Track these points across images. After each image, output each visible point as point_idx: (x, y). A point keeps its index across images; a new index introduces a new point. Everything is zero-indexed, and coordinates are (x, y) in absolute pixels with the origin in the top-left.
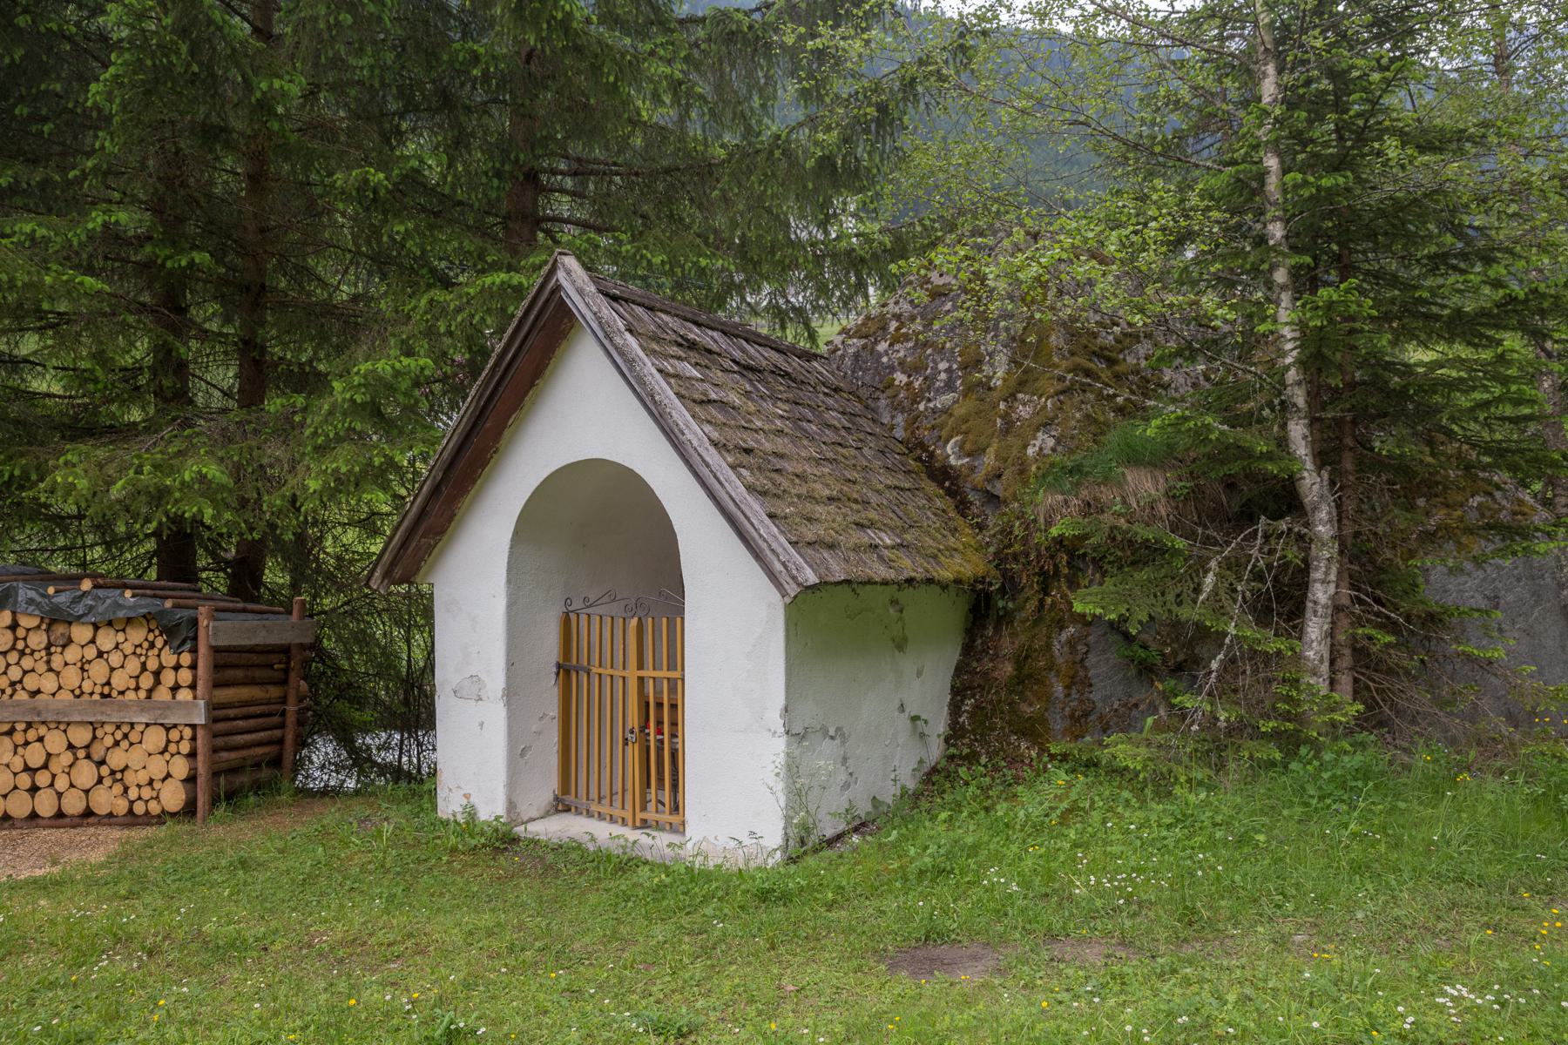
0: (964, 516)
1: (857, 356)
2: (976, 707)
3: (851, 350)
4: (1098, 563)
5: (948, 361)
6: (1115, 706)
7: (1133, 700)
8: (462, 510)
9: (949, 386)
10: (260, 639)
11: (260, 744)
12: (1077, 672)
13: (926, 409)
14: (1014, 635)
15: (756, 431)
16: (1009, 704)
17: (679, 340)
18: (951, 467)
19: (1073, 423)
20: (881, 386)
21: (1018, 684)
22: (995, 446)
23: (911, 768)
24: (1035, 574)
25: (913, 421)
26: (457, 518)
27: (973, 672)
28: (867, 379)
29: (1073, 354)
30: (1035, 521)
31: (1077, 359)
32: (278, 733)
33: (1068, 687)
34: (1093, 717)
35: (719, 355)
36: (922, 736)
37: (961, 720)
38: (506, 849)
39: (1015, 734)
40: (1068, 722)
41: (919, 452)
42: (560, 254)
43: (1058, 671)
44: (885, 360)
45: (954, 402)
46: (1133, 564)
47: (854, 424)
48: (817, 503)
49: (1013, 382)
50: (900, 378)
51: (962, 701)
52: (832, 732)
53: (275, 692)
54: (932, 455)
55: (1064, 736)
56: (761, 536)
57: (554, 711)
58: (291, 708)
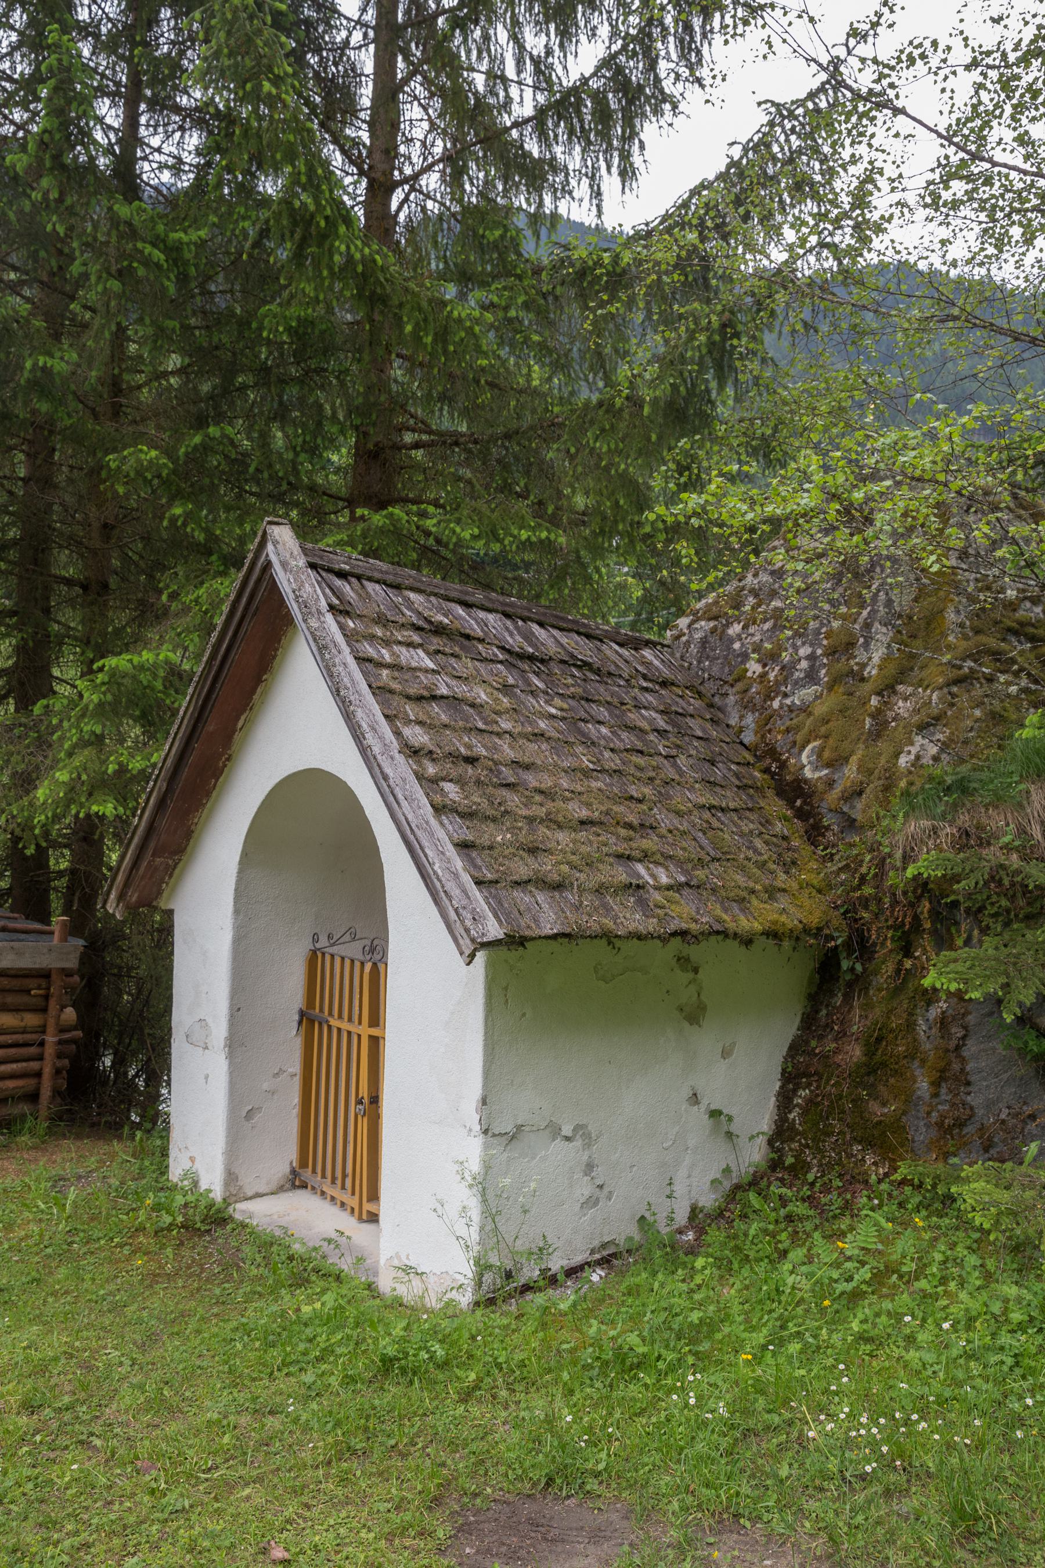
0: (814, 844)
1: (704, 642)
2: (810, 1102)
3: (698, 636)
4: (976, 913)
5: (811, 645)
6: (1003, 1116)
7: (1028, 1110)
8: (199, 827)
9: (811, 677)
10: (26, 962)
11: (12, 1076)
12: (949, 1064)
13: (781, 707)
14: (868, 1006)
15: (498, 734)
16: (853, 1101)
17: (421, 623)
18: (806, 781)
19: (969, 723)
20: (730, 679)
21: (868, 1074)
22: (859, 754)
23: (712, 1177)
24: (888, 928)
25: (766, 722)
26: (195, 835)
27: (812, 1053)
28: (715, 671)
29: (977, 632)
30: (890, 855)
31: (982, 639)
32: (34, 1065)
33: (936, 1084)
34: (970, 1129)
35: (481, 640)
36: (729, 1135)
37: (791, 1116)
38: (208, 1231)
39: (860, 1143)
40: (934, 1133)
41: (768, 761)
42: (270, 523)
43: (923, 1061)
44: (737, 646)
45: (817, 698)
46: (1028, 917)
47: (675, 725)
48: (560, 827)
49: (892, 669)
50: (754, 668)
51: (795, 1091)
52: (567, 1130)
53: (31, 1020)
54: (783, 765)
55: (929, 1150)
56: (435, 872)
57: (295, 1066)
58: (50, 1039)
